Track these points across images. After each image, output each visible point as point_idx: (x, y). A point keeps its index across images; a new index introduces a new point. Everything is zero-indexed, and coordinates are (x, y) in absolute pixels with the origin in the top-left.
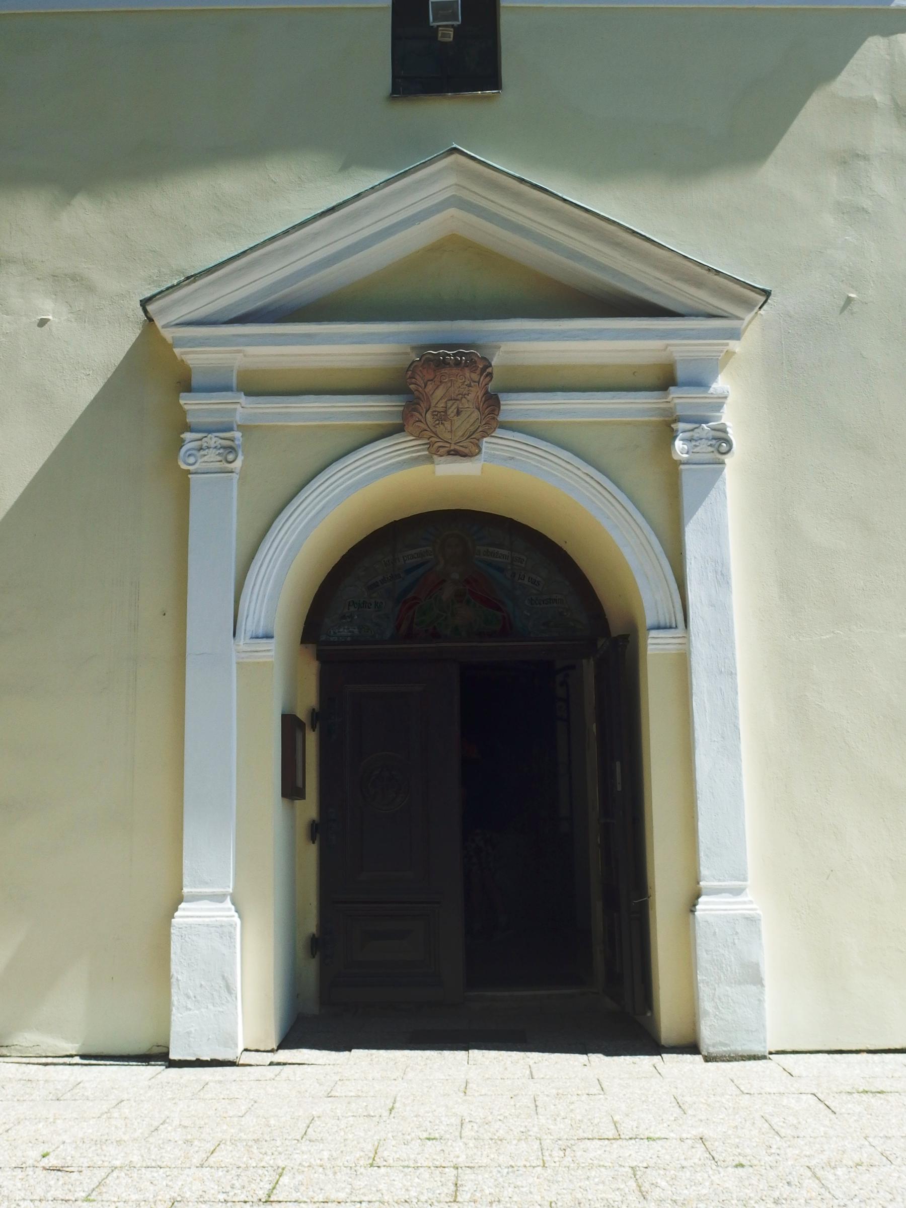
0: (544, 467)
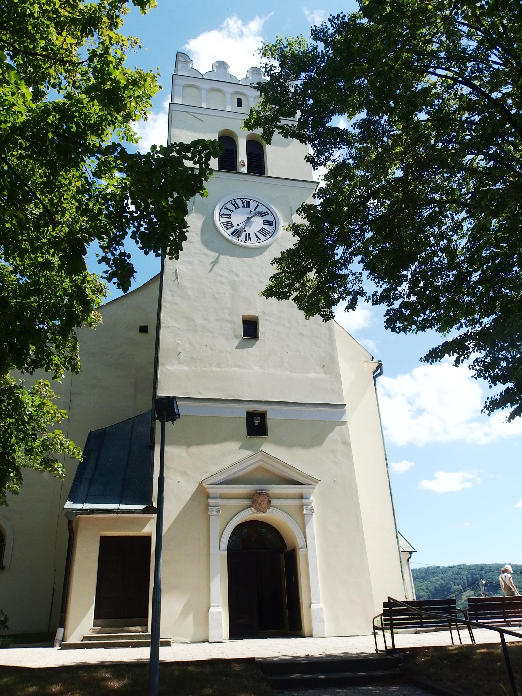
0: (408, 617)
